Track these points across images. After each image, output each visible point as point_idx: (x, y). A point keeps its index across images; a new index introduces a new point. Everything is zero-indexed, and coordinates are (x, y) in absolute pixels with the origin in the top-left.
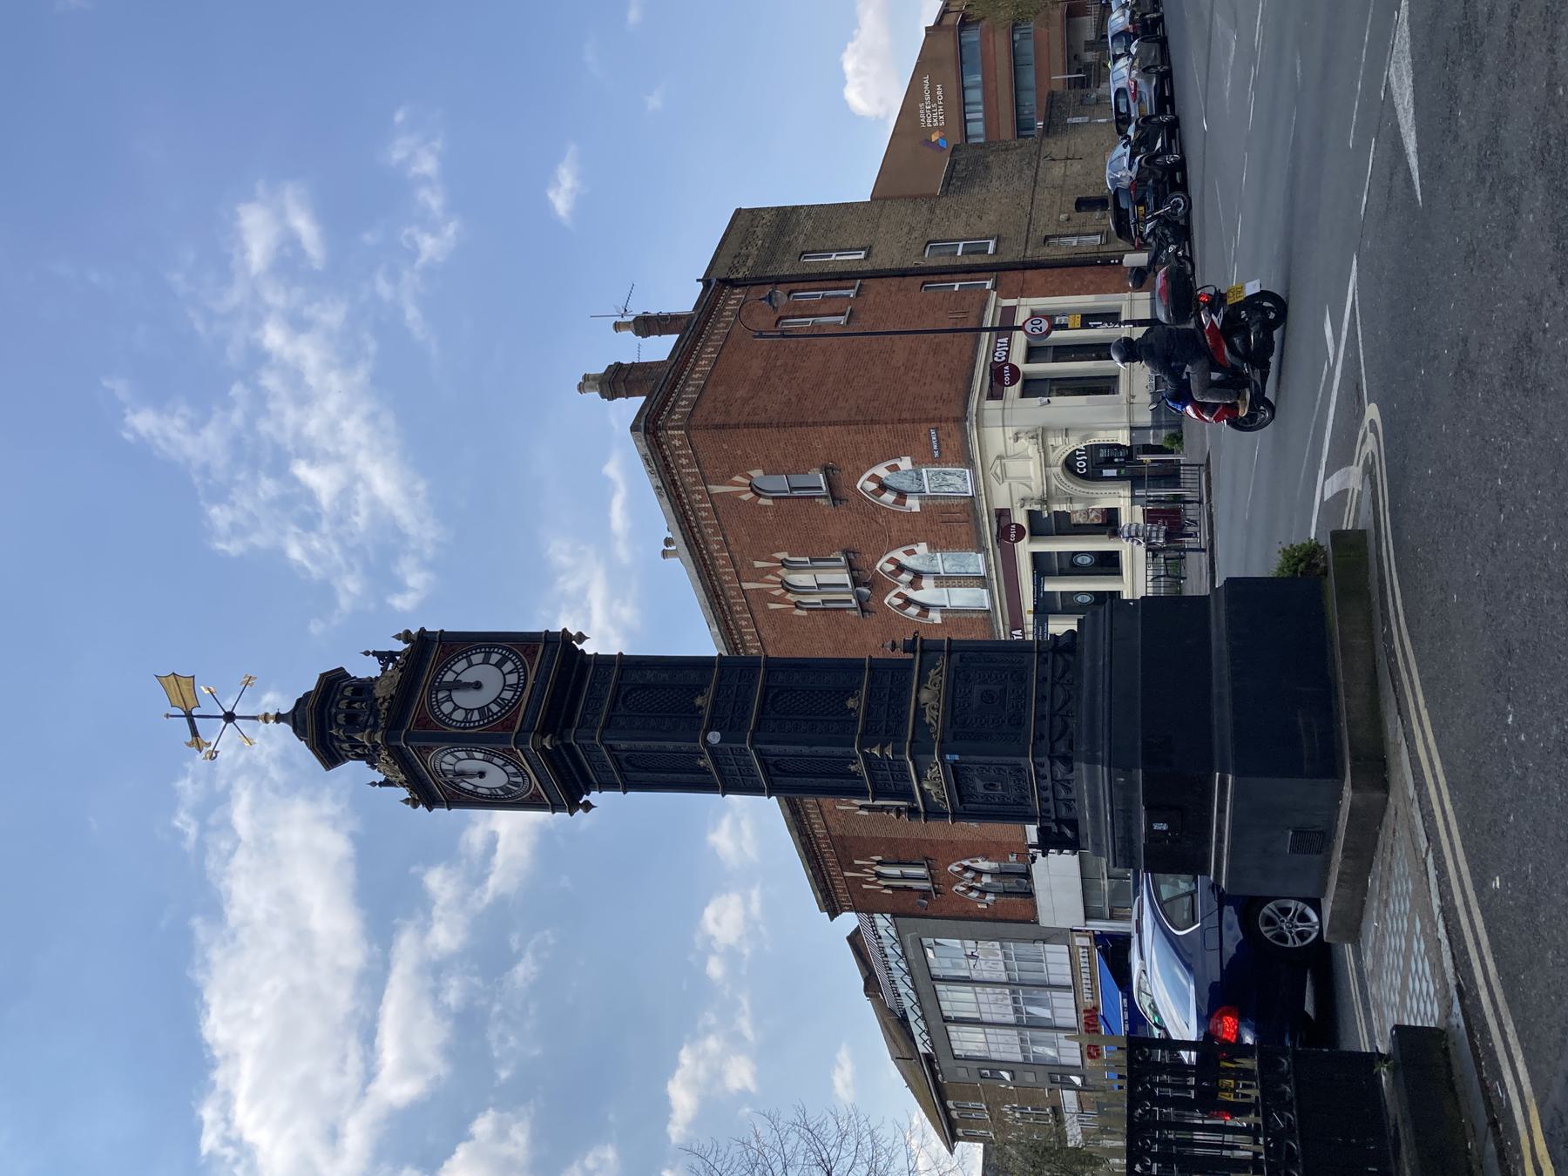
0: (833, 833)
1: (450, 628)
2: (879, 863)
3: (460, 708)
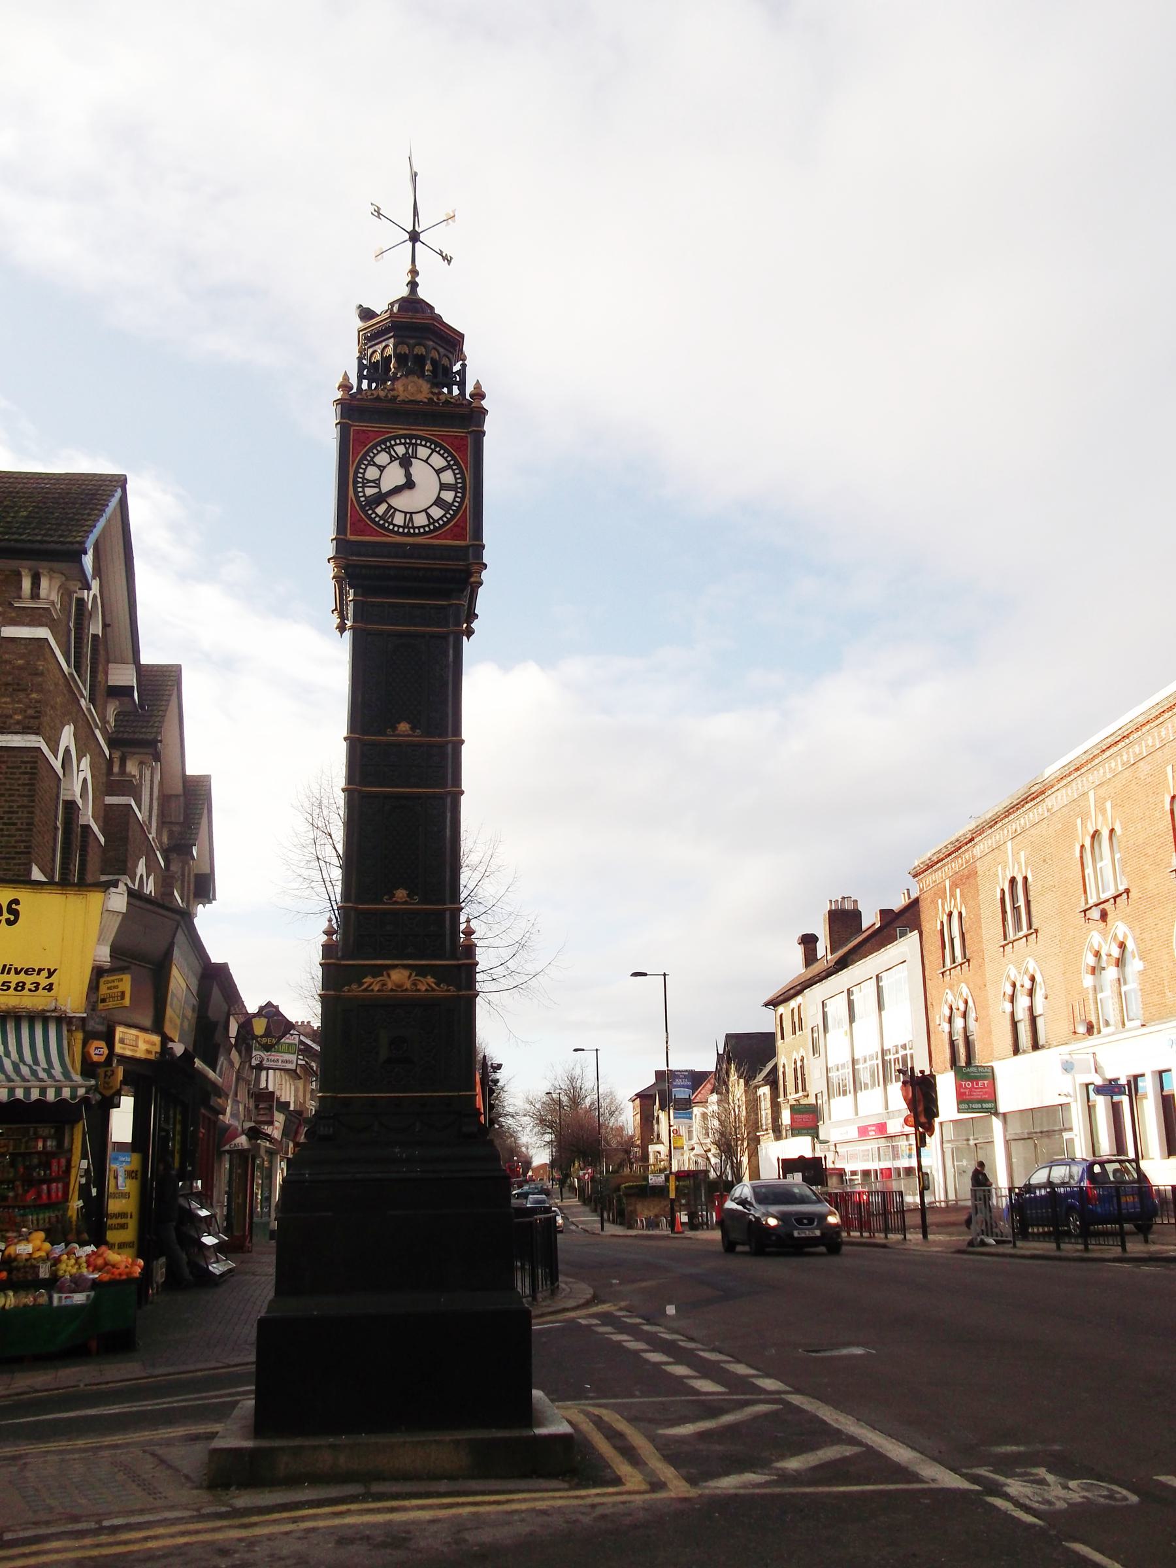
0: (978, 862)
1: (488, 442)
2: (960, 914)
3: (382, 472)
